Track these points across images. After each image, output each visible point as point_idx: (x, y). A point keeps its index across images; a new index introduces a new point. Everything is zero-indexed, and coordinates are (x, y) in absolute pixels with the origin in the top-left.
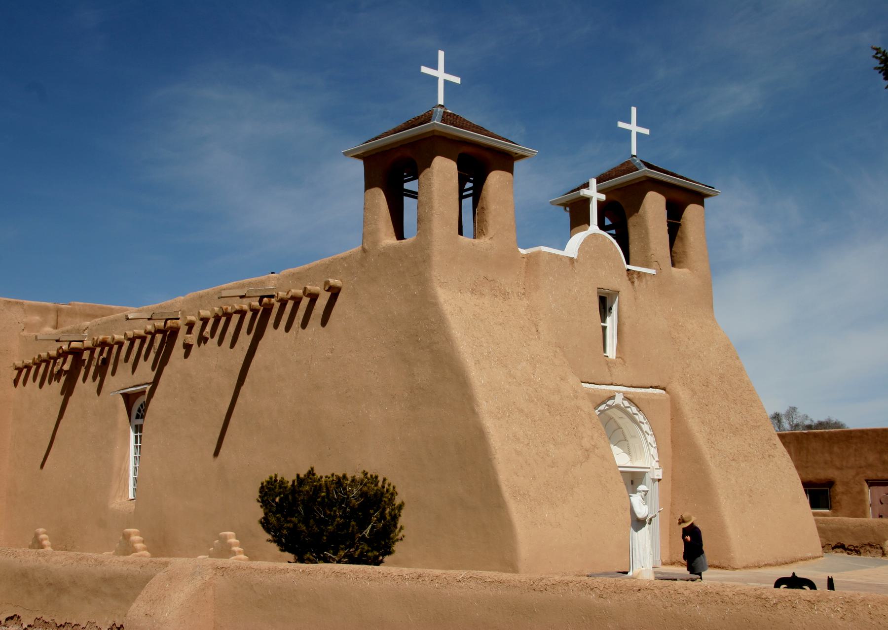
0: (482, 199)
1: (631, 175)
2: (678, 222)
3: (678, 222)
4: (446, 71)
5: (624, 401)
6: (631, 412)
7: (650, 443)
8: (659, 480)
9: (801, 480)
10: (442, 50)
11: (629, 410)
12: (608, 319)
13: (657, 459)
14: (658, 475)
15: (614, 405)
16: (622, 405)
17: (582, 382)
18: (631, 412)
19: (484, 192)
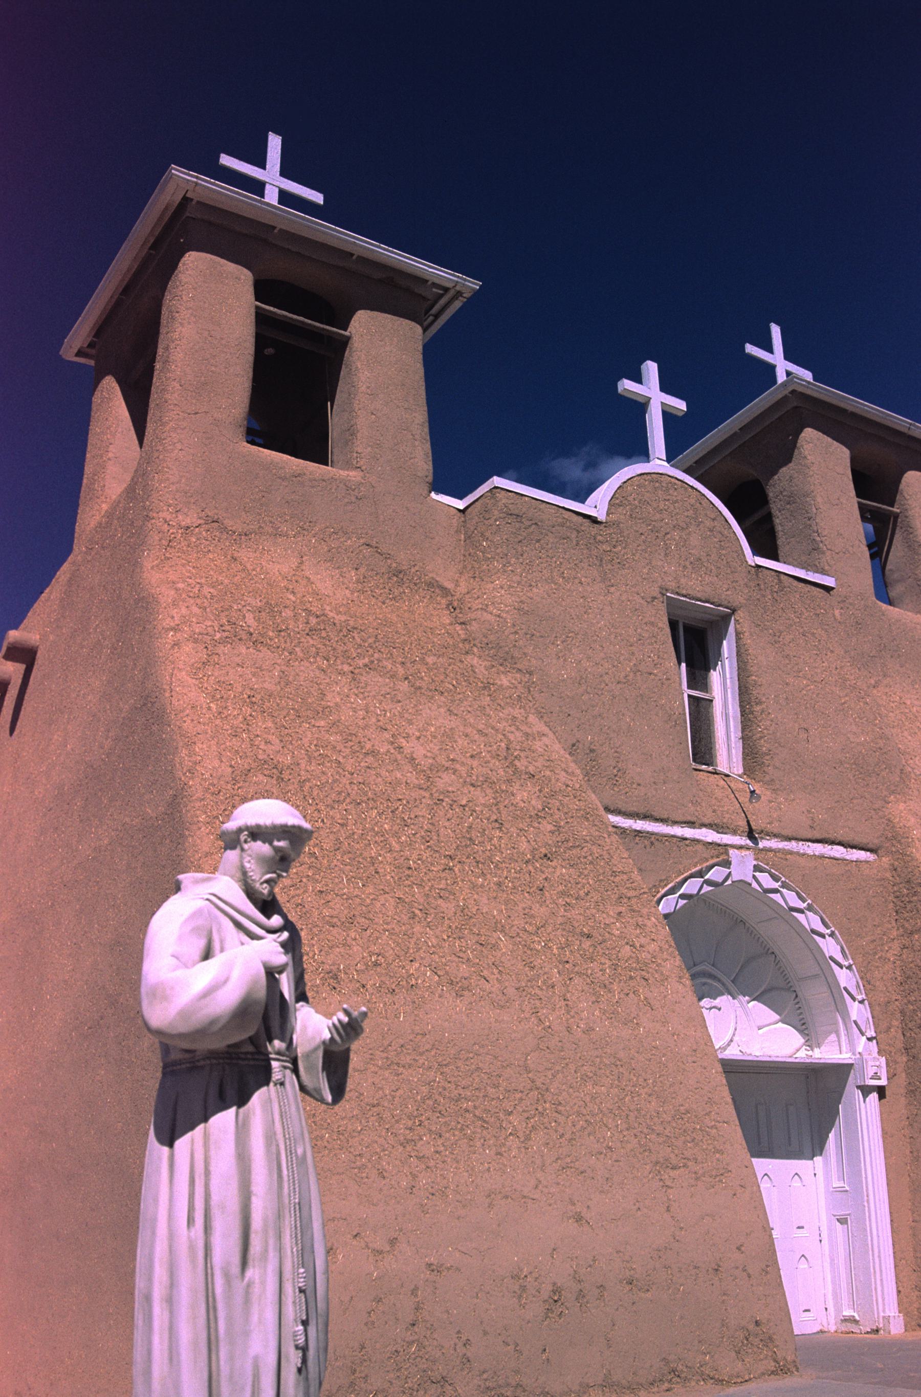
0: (351, 349)
1: (742, 414)
2: (891, 509)
3: (891, 509)
4: (284, 173)
5: (757, 874)
6: (783, 904)
7: (845, 989)
8: (881, 1091)
9: (669, 614)
10: (277, 132)
11: (776, 897)
12: (715, 676)
13: (871, 1033)
14: (876, 1077)
15: (729, 882)
16: (755, 885)
17: (608, 810)
18: (783, 904)
19: (144, 973)
